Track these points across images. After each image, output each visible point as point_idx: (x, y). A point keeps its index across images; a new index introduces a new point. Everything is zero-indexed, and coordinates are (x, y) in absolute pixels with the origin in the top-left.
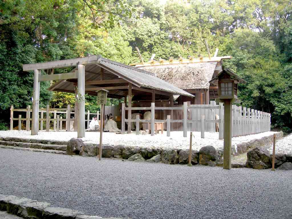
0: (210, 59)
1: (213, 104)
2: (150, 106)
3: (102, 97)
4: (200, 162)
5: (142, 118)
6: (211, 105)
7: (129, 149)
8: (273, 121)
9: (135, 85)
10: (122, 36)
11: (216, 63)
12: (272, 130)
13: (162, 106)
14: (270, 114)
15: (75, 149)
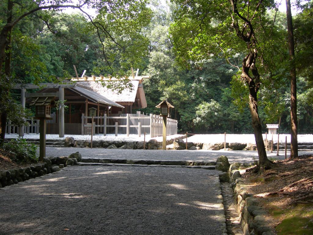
0: (134, 78)
3: (93, 112)
4: (149, 148)
7: (107, 142)
8: (179, 126)
10: (56, 52)
12: (178, 133)
14: (177, 121)
15: (70, 143)
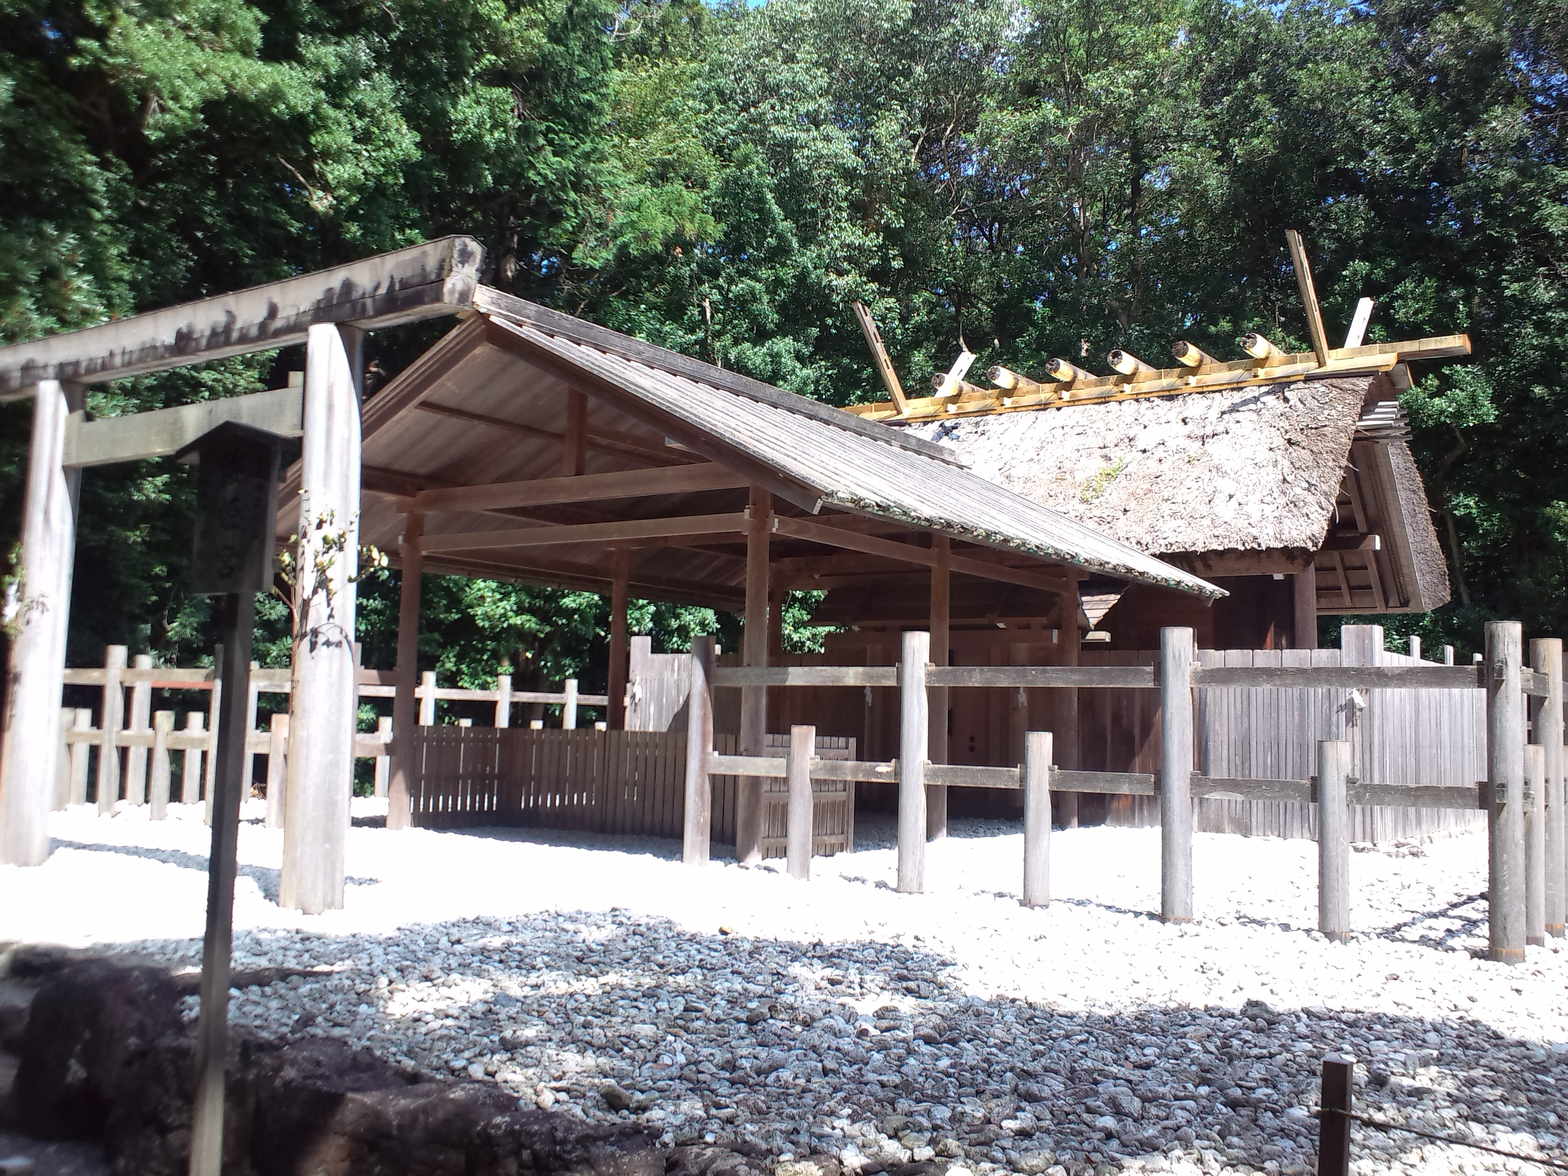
1: (1365, 650)
2: (893, 656)
5: (719, 784)
6: (1347, 656)
9: (1542, 909)
11: (1363, 384)
13: (1007, 661)
